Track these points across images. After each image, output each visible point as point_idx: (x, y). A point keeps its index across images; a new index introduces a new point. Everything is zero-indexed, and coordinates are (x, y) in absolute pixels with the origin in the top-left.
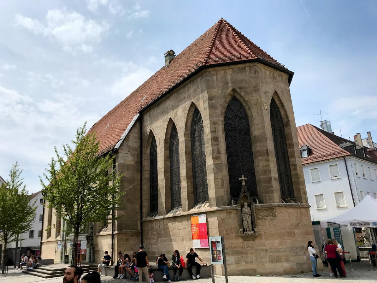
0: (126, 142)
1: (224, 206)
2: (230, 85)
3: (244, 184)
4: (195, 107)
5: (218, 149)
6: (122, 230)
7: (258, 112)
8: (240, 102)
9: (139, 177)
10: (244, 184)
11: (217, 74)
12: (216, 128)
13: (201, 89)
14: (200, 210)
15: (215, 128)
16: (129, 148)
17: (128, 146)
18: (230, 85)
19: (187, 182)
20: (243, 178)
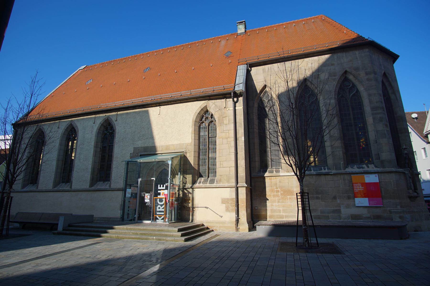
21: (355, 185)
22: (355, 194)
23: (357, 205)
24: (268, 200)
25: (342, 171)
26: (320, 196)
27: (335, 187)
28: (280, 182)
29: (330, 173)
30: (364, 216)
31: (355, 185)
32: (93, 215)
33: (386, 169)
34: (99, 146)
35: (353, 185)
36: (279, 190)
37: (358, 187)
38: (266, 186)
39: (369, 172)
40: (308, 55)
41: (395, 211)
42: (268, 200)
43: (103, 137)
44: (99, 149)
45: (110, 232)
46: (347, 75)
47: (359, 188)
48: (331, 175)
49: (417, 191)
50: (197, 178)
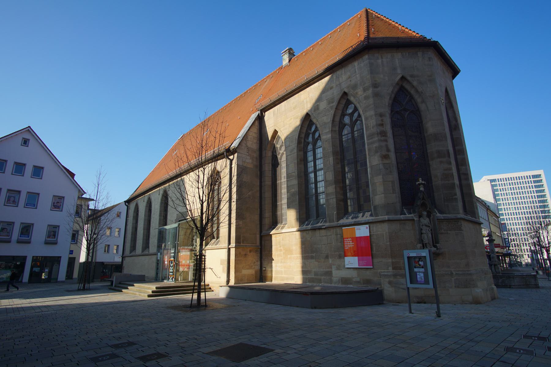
0: (244, 142)
1: (397, 215)
2: (399, 71)
3: (422, 189)
4: (346, 99)
5: (387, 146)
6: (240, 243)
7: (435, 106)
8: (410, 93)
9: (258, 184)
10: (422, 189)
11: (382, 56)
12: (383, 121)
13: (360, 75)
14: (359, 221)
15: (382, 120)
16: (248, 149)
17: (247, 146)
18: (399, 71)
19: (336, 188)
20: (420, 181)
21: (346, 241)
22: (345, 252)
23: (346, 267)
24: (274, 260)
25: (335, 224)
26: (314, 255)
27: (328, 244)
28: (283, 240)
29: (322, 227)
30: (354, 280)
31: (346, 241)
32: (145, 275)
33: (378, 217)
34: (163, 215)
35: (344, 241)
36: (281, 249)
37: (349, 243)
38: (273, 245)
39: (359, 223)
40: (308, 83)
41: (386, 273)
42: (274, 260)
43: (165, 206)
44: (163, 217)
45: (129, 288)
46: (348, 98)
47: (349, 244)
48: (324, 228)
49: (437, 245)
50: (209, 240)
